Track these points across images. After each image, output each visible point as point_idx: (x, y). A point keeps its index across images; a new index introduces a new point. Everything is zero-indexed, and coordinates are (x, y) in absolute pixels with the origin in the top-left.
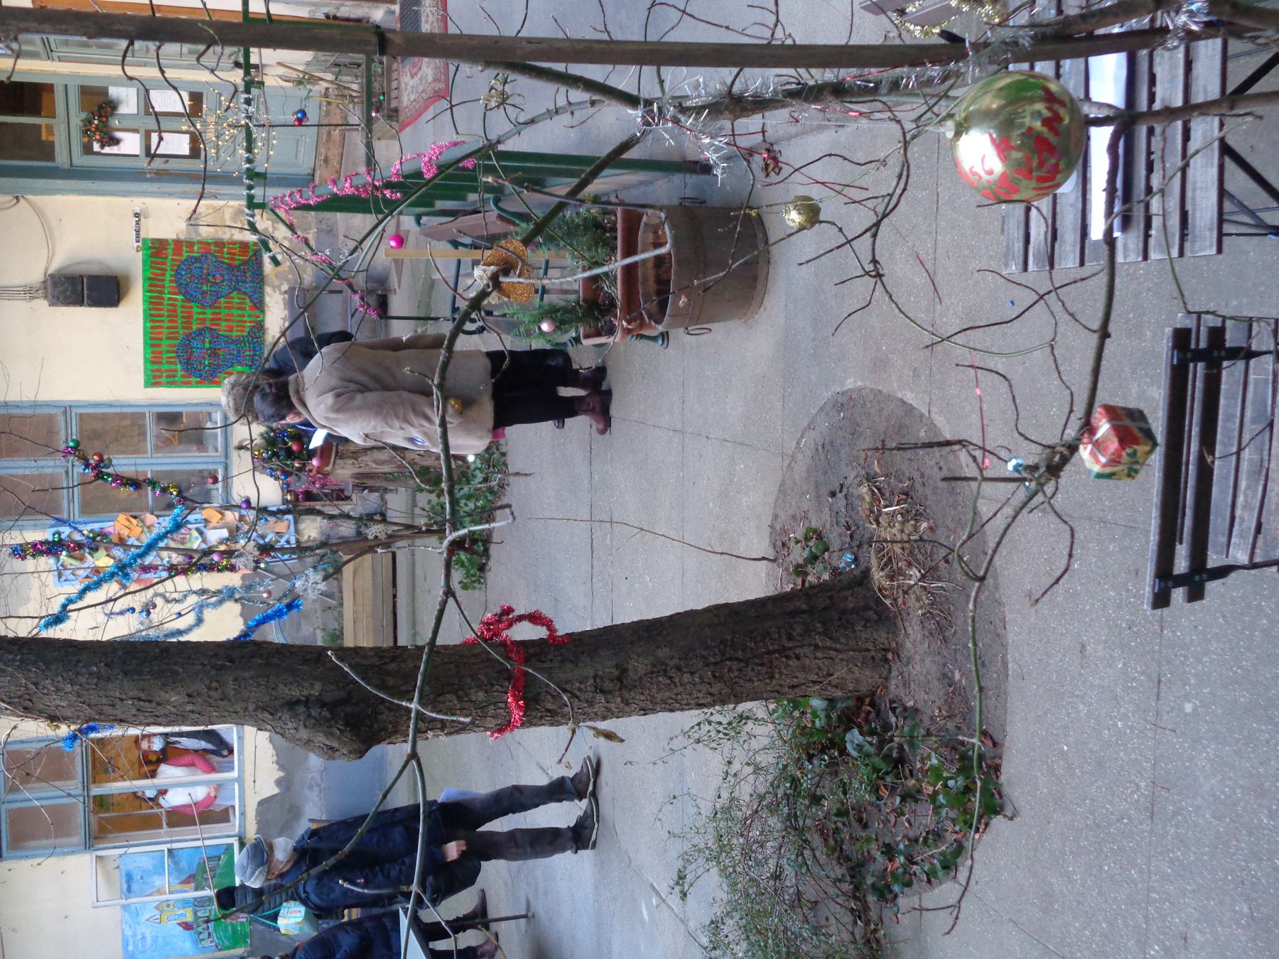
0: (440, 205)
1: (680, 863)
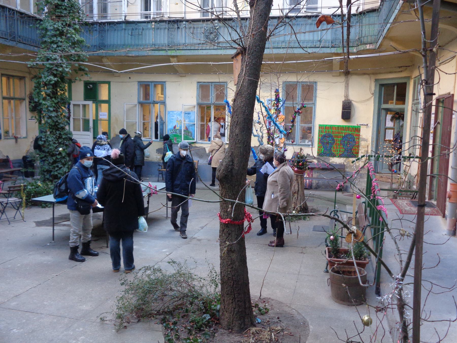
0: (368, 209)
1: (177, 262)
